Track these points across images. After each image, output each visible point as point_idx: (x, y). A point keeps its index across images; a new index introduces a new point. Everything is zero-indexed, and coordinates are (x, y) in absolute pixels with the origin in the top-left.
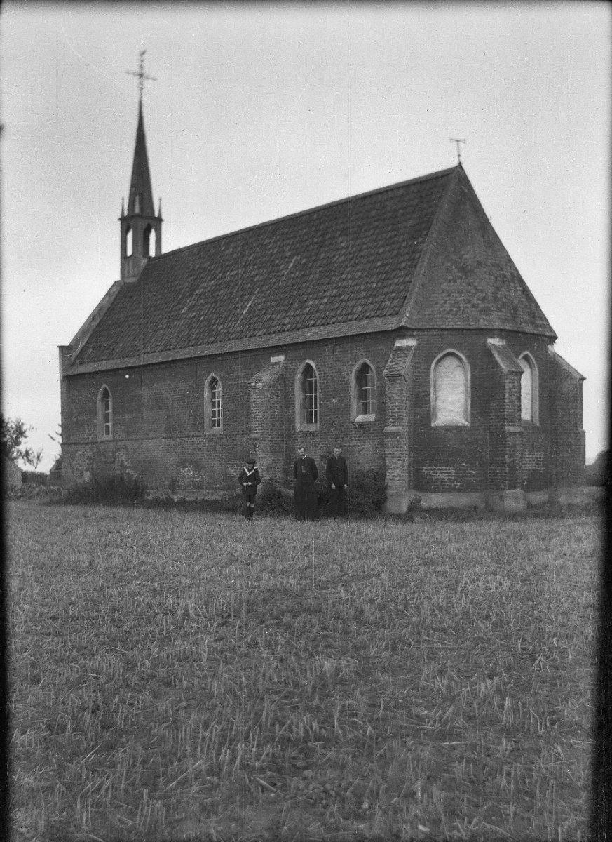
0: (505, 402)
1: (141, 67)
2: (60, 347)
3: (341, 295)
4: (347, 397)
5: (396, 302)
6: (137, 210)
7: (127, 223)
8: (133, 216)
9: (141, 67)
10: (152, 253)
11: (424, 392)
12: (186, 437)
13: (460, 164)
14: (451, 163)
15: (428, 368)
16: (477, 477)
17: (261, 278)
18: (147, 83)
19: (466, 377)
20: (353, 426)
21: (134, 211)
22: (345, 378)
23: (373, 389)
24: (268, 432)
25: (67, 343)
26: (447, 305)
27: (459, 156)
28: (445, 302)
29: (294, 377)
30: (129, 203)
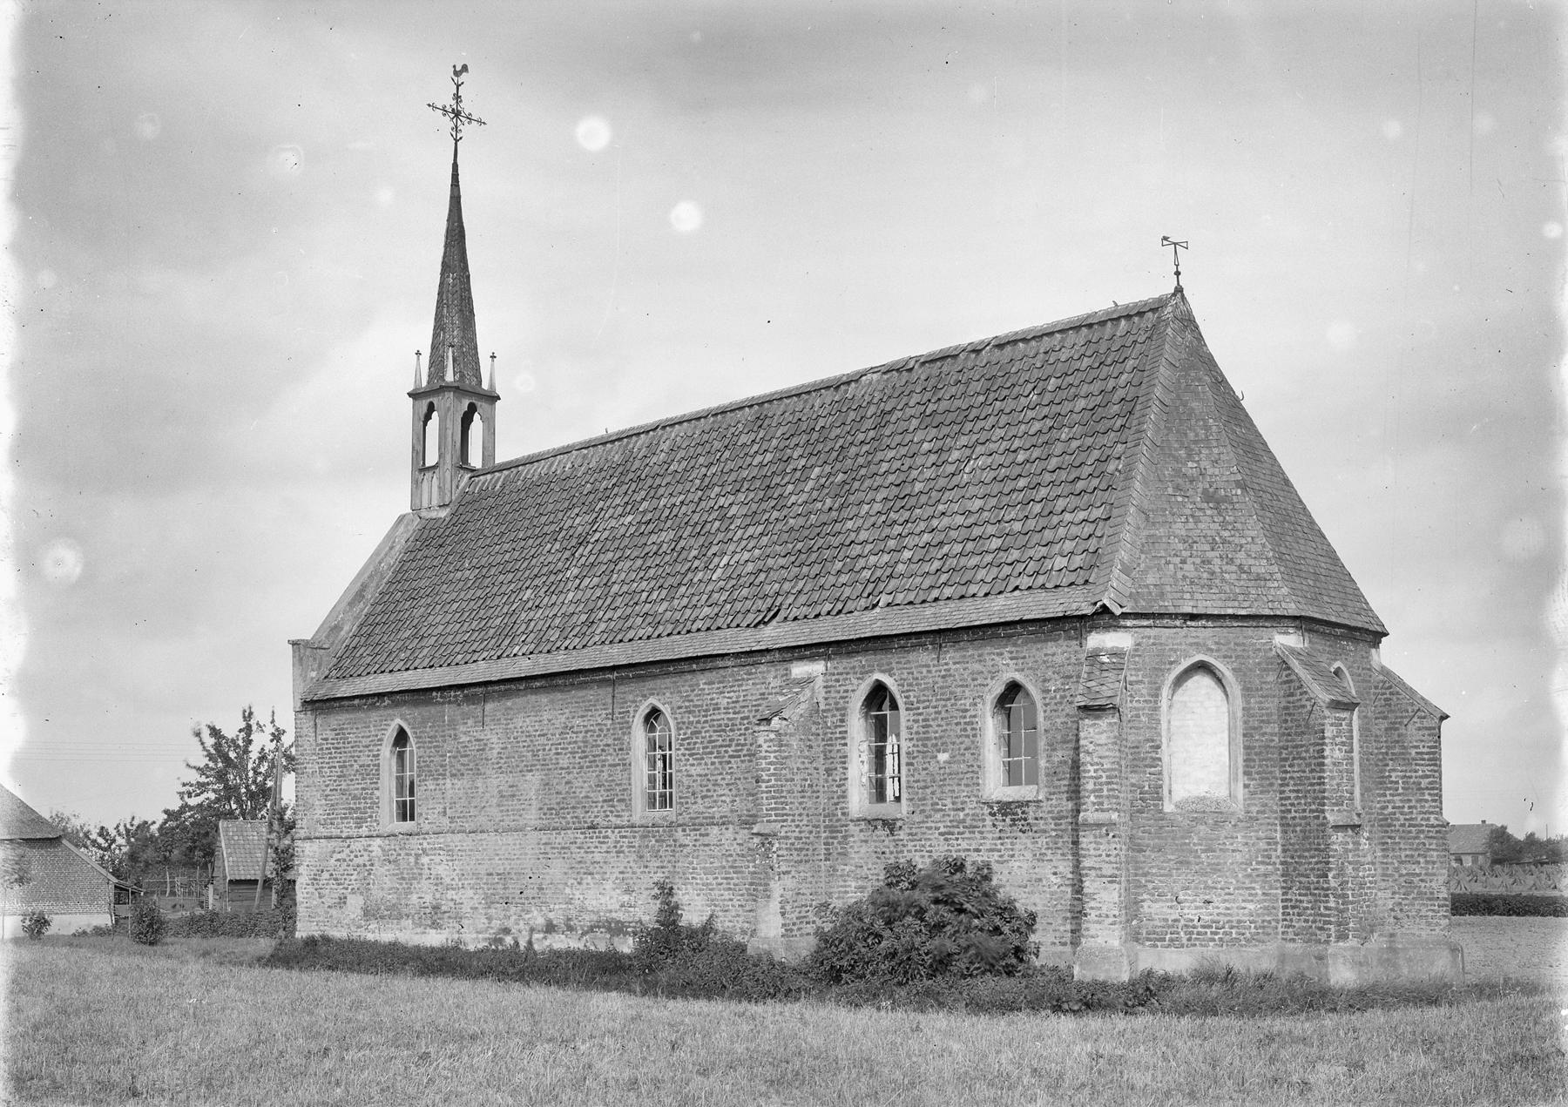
0: (1323, 764)
1: (457, 97)
2: (294, 644)
3: (941, 543)
4: (975, 750)
5: (1078, 561)
6: (450, 377)
7: (425, 398)
8: (441, 387)
9: (457, 97)
10: (475, 460)
11: (1148, 740)
12: (589, 828)
13: (1179, 290)
14: (1149, 287)
15: (1156, 694)
16: (1258, 915)
17: (744, 510)
18: (467, 130)
19: (1232, 716)
20: (986, 810)
21: (442, 378)
22: (967, 711)
23: (1403, 783)
24: (793, 821)
25: (307, 635)
26: (1189, 567)
27: (1178, 273)
28: (1184, 562)
29: (845, 709)
30: (432, 364)
